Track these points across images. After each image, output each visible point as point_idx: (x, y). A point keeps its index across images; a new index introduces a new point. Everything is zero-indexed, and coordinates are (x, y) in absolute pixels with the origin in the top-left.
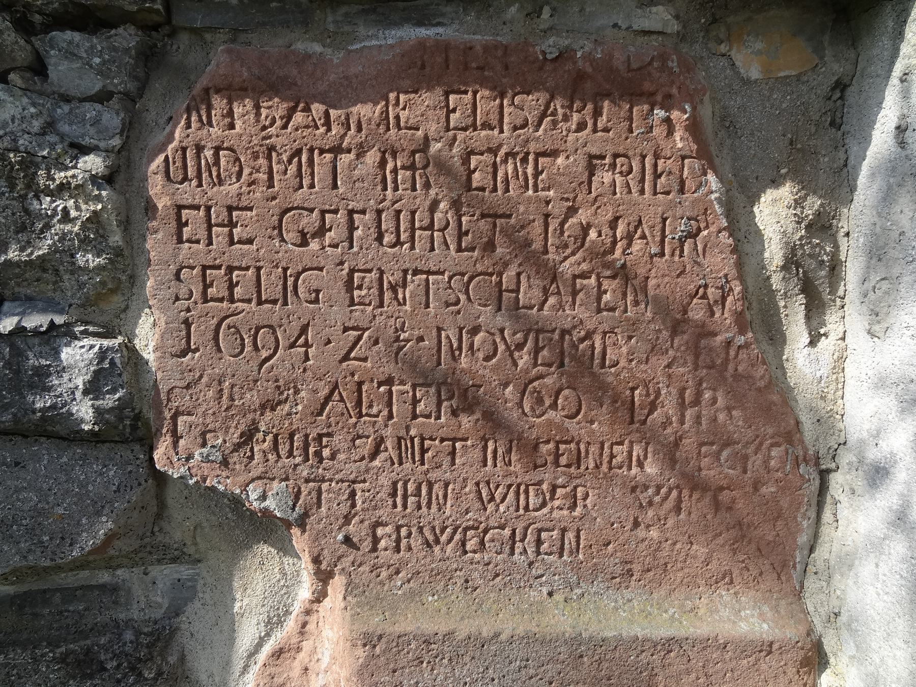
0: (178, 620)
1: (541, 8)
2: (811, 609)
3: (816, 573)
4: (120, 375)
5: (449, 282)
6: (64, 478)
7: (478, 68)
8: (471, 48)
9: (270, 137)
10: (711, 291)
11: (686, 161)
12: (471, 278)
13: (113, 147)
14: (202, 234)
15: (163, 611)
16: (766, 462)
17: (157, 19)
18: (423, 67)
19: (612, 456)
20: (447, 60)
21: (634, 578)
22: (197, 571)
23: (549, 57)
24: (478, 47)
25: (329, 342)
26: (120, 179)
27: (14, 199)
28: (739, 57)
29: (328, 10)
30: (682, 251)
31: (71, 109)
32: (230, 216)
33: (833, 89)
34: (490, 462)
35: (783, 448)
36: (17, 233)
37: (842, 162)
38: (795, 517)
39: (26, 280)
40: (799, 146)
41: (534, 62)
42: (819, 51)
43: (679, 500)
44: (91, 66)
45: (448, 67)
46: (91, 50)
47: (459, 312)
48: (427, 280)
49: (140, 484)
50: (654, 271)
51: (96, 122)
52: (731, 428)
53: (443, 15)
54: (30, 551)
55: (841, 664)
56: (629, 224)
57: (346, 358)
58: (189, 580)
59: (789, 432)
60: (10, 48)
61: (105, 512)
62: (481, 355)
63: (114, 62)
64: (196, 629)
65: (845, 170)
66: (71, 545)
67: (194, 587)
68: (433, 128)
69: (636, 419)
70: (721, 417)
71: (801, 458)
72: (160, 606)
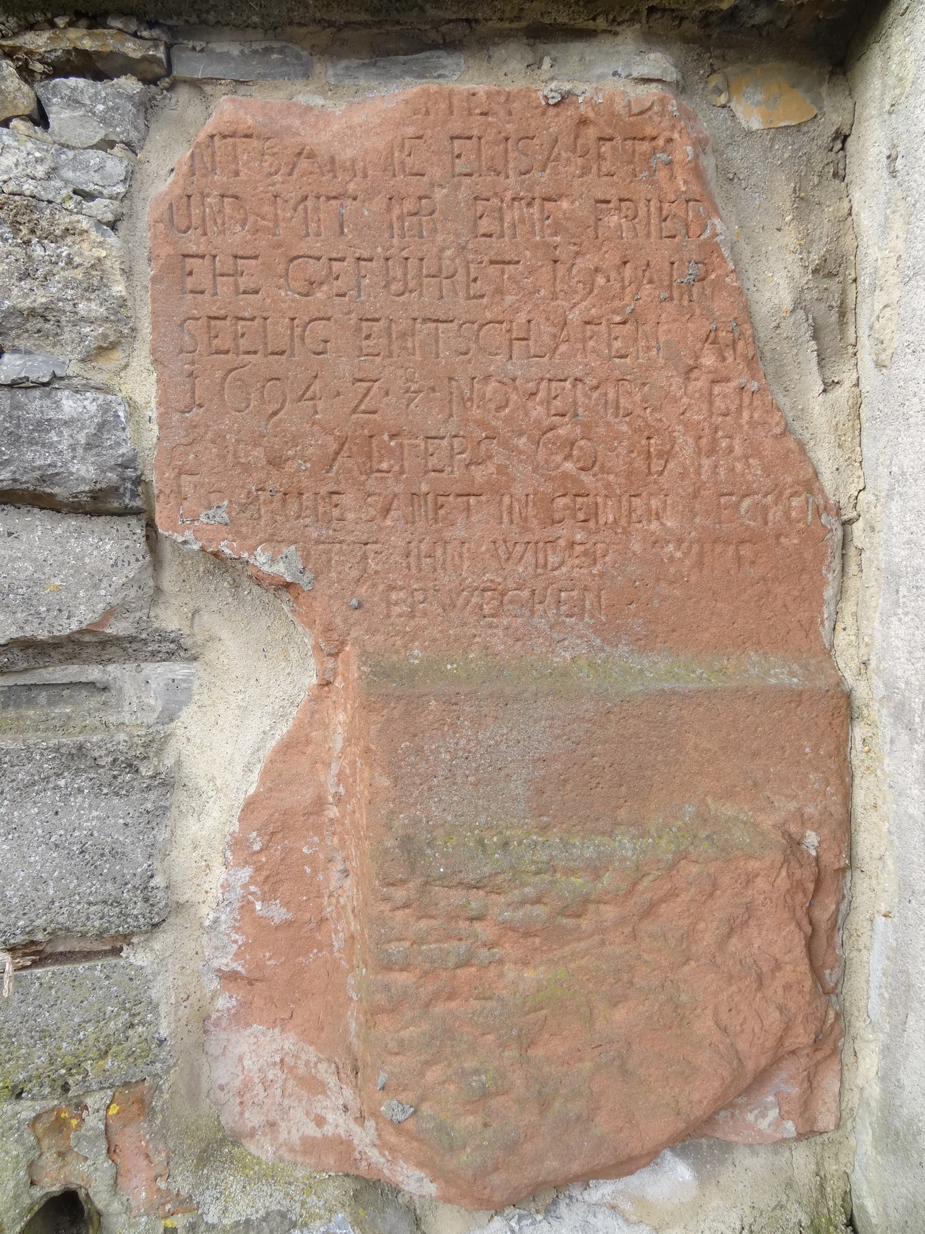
0: (173, 725)
1: (541, 60)
2: (841, 665)
3: (844, 629)
4: (124, 429)
5: (459, 330)
6: (60, 550)
7: (482, 114)
8: (474, 95)
9: (274, 184)
10: (722, 334)
11: (691, 204)
12: (482, 326)
13: (118, 194)
14: (207, 284)
15: (156, 715)
16: (787, 513)
17: (158, 70)
18: (427, 113)
19: (631, 511)
20: (451, 106)
21: (659, 640)
22: (193, 671)
23: (552, 102)
24: (482, 93)
25: (338, 394)
26: (122, 226)
27: (18, 245)
28: (738, 107)
29: (329, 64)
30: (691, 295)
31: (75, 156)
32: (236, 264)
33: (834, 139)
34: (506, 518)
35: (803, 497)
36: (20, 279)
37: (846, 211)
38: (820, 571)
39: (27, 331)
40: (802, 194)
41: (536, 108)
42: (817, 101)
43: (701, 554)
44: (94, 114)
45: (452, 113)
46: (95, 98)
47: (469, 362)
48: (437, 329)
49: (137, 560)
50: (664, 315)
51: (100, 169)
52: (750, 478)
53: (444, 67)
54: (26, 622)
55: (873, 713)
56: (636, 269)
57: (354, 411)
58: (184, 681)
59: (809, 480)
60: (12, 95)
61: (102, 586)
62: (493, 406)
63: (118, 109)
64: (193, 733)
65: (850, 219)
66: (69, 618)
67: (189, 689)
68: (436, 172)
69: (653, 470)
70: (739, 467)
71: (822, 507)
72: (153, 709)
